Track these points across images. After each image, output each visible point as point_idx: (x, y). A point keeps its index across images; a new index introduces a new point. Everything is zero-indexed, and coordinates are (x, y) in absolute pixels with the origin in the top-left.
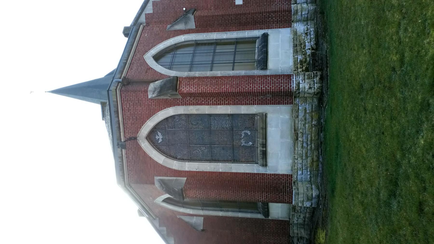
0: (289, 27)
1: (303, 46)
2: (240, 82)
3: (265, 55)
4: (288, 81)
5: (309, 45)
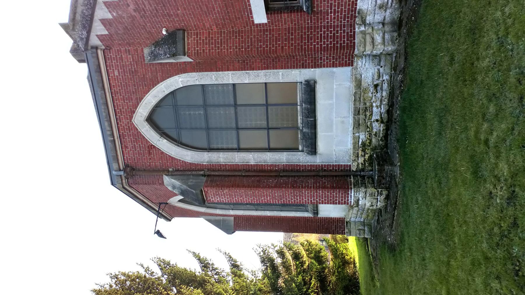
0: (349, 65)
1: (368, 114)
2: (283, 194)
3: (313, 131)
4: (345, 195)
5: (378, 111)
